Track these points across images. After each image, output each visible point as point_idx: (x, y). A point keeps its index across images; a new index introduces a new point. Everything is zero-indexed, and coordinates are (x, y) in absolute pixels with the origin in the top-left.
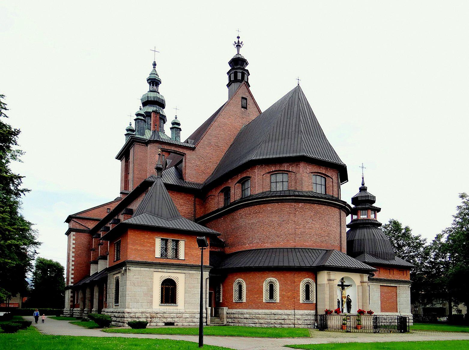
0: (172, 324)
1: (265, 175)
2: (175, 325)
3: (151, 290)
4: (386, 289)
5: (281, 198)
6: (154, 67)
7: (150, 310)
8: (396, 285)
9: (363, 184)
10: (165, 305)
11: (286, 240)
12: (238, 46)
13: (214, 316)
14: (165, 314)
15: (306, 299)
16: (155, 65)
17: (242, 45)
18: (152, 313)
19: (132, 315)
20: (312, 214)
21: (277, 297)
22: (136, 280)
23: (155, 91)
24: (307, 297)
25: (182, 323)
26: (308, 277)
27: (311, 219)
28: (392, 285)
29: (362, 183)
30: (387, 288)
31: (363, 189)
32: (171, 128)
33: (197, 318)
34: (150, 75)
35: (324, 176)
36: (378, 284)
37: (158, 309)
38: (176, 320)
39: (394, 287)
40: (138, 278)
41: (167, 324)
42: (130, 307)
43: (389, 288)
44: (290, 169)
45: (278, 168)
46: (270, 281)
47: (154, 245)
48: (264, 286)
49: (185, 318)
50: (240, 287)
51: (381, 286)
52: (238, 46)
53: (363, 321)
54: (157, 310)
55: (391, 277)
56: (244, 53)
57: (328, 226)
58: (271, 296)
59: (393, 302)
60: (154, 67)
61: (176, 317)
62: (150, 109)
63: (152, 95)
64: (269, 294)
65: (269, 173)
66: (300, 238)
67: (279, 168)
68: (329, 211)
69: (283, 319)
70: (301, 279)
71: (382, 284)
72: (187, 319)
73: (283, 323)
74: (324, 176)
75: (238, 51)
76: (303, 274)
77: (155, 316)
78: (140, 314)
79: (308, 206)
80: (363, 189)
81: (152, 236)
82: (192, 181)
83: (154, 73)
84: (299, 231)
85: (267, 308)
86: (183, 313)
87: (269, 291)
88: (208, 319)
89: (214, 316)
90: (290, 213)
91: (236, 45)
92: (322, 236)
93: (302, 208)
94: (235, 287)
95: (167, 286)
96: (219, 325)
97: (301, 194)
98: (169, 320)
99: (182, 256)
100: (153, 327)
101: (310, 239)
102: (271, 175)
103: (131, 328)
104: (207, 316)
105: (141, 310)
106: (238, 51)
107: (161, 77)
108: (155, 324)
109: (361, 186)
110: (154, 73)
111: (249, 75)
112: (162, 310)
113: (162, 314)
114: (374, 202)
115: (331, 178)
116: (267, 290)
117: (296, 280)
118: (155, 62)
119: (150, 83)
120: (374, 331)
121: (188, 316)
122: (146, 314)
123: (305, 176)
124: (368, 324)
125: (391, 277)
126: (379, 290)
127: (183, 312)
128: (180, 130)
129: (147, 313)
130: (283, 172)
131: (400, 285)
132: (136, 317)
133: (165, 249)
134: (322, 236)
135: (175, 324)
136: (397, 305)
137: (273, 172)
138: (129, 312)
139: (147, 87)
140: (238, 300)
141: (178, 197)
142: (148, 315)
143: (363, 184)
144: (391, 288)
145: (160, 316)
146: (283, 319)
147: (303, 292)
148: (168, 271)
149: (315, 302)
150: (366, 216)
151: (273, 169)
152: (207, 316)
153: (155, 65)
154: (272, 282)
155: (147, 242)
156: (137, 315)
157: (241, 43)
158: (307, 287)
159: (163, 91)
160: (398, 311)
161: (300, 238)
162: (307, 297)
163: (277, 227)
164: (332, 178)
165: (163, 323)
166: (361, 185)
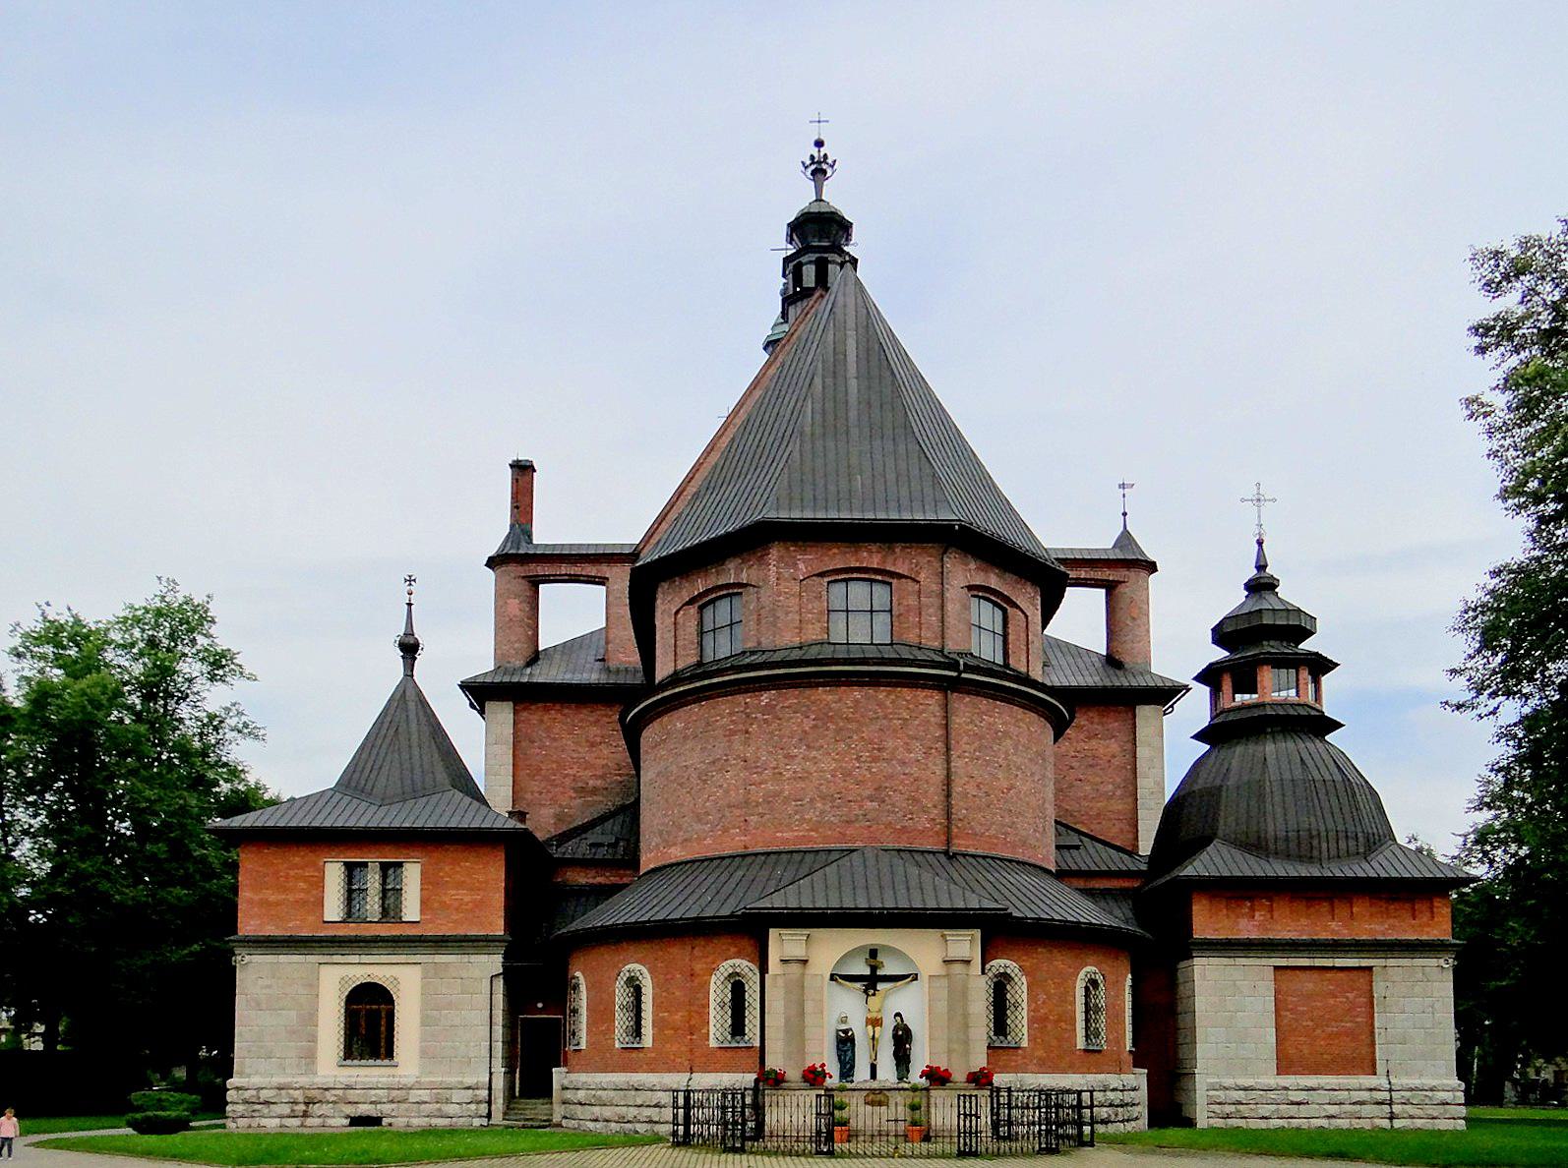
0: (375, 1121)
1: (681, 612)
2: (383, 1124)
3: (310, 1018)
4: (1308, 984)
5: (698, 684)
7: (304, 1081)
8: (1365, 963)
9: (1261, 567)
10: (363, 1062)
11: (719, 827)
12: (819, 170)
13: (522, 1095)
14: (352, 1091)
15: (733, 1035)
18: (309, 1089)
19: (247, 1094)
20: (808, 725)
22: (264, 991)
24: (738, 1028)
25: (406, 1120)
26: (738, 955)
27: (804, 742)
28: (1339, 962)
29: (1257, 563)
30: (1315, 975)
31: (1261, 585)
33: (458, 1103)
34: (772, 329)
35: (879, 578)
36: (1264, 961)
37: (328, 1076)
38: (386, 1108)
39: (494, 985)
40: (269, 987)
41: (356, 1121)
42: (247, 1071)
43: (1329, 975)
44: (744, 578)
45: (713, 580)
46: (1002, 971)
47: (319, 883)
48: (713, 987)
49: (418, 1103)
50: (638, 992)
51: (1276, 968)
52: (819, 170)
53: (264, 1122)
54: (326, 1080)
55: (1334, 928)
56: (838, 197)
57: (875, 760)
59: (1351, 1034)
61: (385, 1100)
65: (692, 601)
66: (762, 815)
67: (714, 579)
68: (880, 704)
69: (656, 1106)
70: (713, 963)
71: (1283, 962)
72: (423, 1105)
73: (657, 1119)
74: (879, 578)
75: (819, 190)
76: (722, 943)
77: (319, 1098)
78: (273, 1093)
79: (792, 697)
80: (1261, 585)
81: (311, 857)
82: (629, 662)
84: (756, 793)
85: (624, 1069)
86: (411, 1089)
88: (493, 1107)
89: (522, 1095)
90: (733, 733)
91: (813, 167)
92: (850, 801)
93: (769, 708)
94: (621, 995)
95: (374, 1007)
96: (524, 1127)
97: (777, 657)
98: (365, 1110)
99: (411, 910)
100: (314, 1131)
101: (797, 817)
102: (701, 609)
103: (135, 1132)
104: (490, 1095)
105: (278, 1080)
106: (819, 190)
108: (317, 1121)
109: (1252, 572)
112: (342, 1080)
113: (340, 1093)
114: (1307, 633)
115: (911, 578)
116: (722, 1004)
117: (698, 967)
120: (1040, 1144)
121: (425, 1095)
122: (291, 1091)
123: (786, 593)
124: (796, 1124)
125: (1334, 928)
127: (409, 1086)
129: (296, 1089)
130: (731, 591)
131: (1391, 962)
132: (261, 1100)
133: (352, 894)
134: (850, 801)
135: (385, 1121)
136: (1373, 1044)
137: (701, 595)
138: (239, 1085)
140: (627, 1039)
141: (581, 721)
142: (298, 1095)
143: (1261, 567)
144: (1341, 975)
145: (335, 1099)
146: (656, 1106)
148: (365, 959)
149: (757, 1044)
150: (1293, 692)
151: (701, 586)
152: (490, 1095)
154: (738, 974)
155: (297, 878)
156: (264, 1095)
157: (832, 166)
158: (738, 989)
160: (1380, 1068)
161: (762, 815)
162: (738, 1028)
163: (698, 784)
164: (914, 580)
165: (346, 1118)
166: (1255, 572)
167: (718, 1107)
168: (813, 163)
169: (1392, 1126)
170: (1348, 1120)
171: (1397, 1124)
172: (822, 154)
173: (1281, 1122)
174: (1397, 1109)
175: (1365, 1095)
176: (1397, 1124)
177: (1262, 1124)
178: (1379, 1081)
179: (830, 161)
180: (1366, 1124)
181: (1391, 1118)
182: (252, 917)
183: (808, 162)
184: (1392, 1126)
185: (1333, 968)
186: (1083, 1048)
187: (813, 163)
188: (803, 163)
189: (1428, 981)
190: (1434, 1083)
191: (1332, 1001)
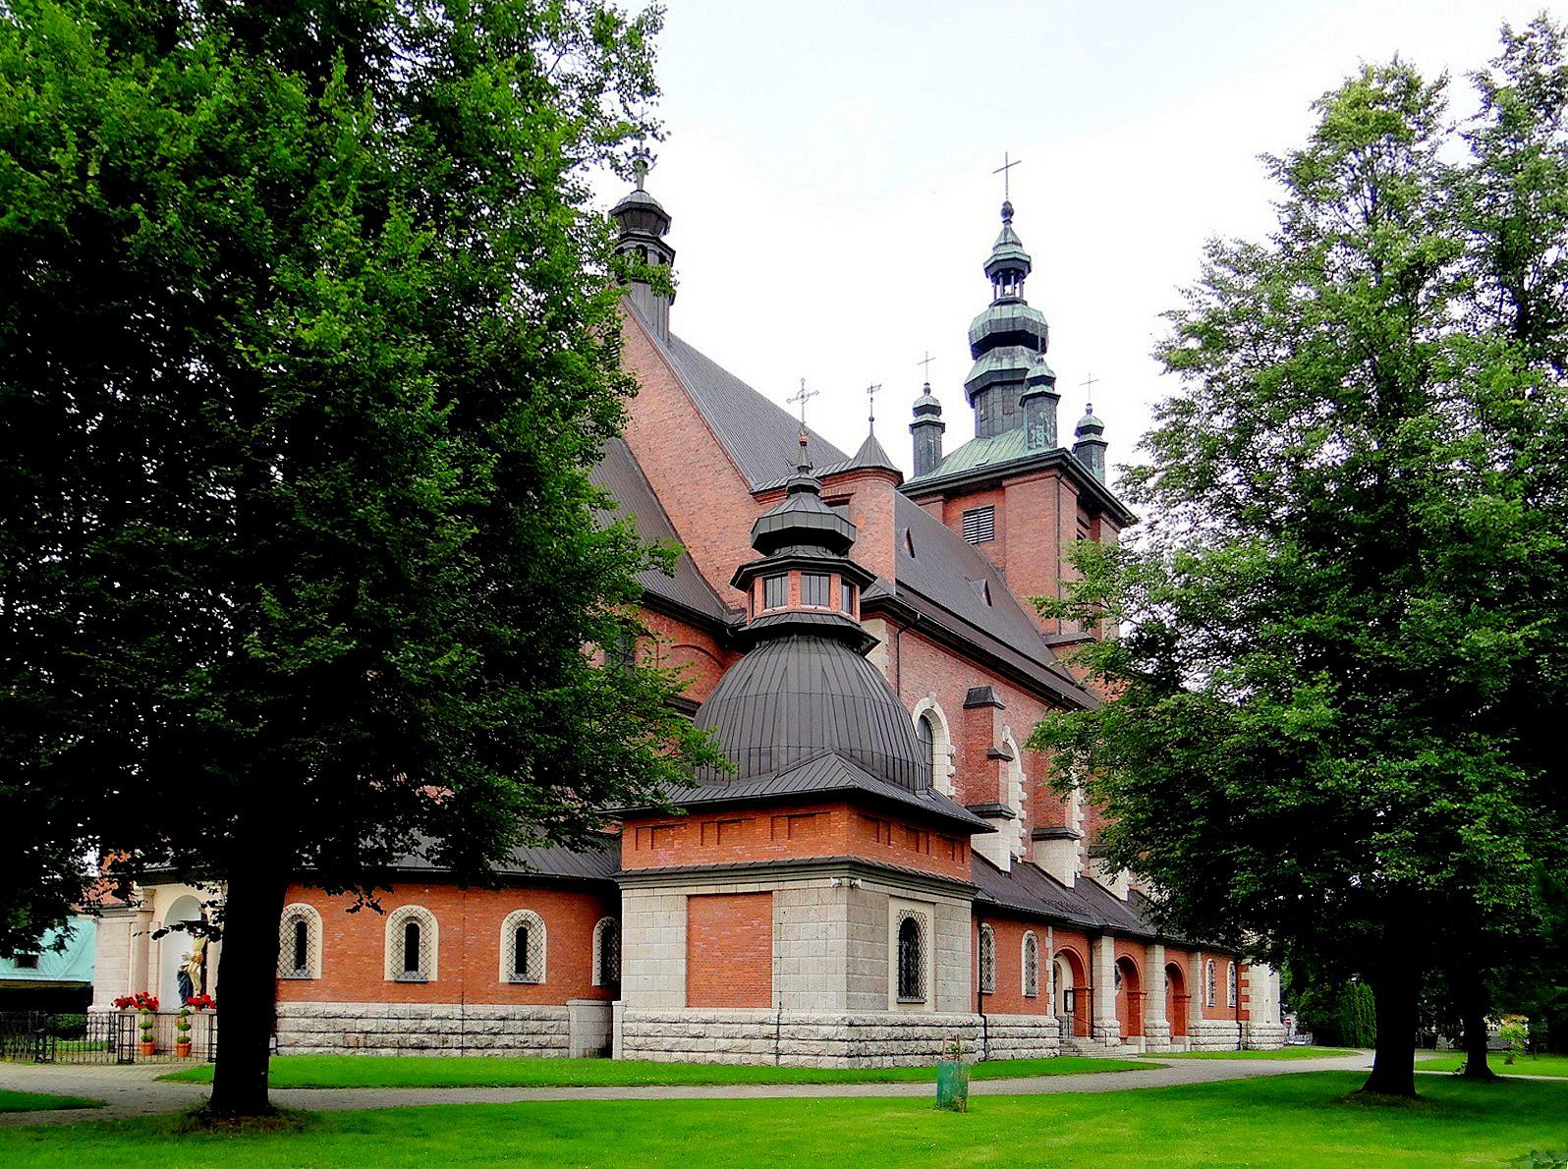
4: (719, 910)
6: (1008, 222)
8: (764, 888)
15: (298, 967)
16: (1008, 212)
17: (653, 160)
21: (539, 966)
23: (1013, 302)
28: (741, 889)
30: (725, 902)
32: (913, 426)
36: (678, 891)
51: (689, 897)
58: (412, 961)
60: (1008, 222)
62: (1000, 361)
63: (1007, 312)
64: (403, 954)
71: (693, 891)
83: (1009, 239)
87: (403, 947)
107: (1029, 249)
110: (1009, 239)
111: (674, 252)
118: (1007, 204)
119: (995, 278)
126: (680, 917)
128: (942, 426)
139: (986, 291)
147: (427, 941)
148: (911, 894)
153: (1008, 212)
157: (653, 160)
159: (1038, 294)
160: (775, 1003)
167: (956, 1052)
168: (635, 154)
169: (777, 1063)
170: (738, 1055)
171: (783, 1060)
172: (644, 148)
173: (306, 1050)
174: (782, 1044)
175: (753, 1029)
176: (783, 1060)
177: (664, 1057)
178: (770, 1014)
179: (652, 155)
180: (754, 1060)
181: (778, 1055)
182: (82, 853)
183: (631, 153)
184: (777, 1063)
185: (736, 895)
186: (507, 981)
187: (635, 154)
188: (626, 154)
189: (823, 904)
190: (816, 1015)
191: (738, 929)
